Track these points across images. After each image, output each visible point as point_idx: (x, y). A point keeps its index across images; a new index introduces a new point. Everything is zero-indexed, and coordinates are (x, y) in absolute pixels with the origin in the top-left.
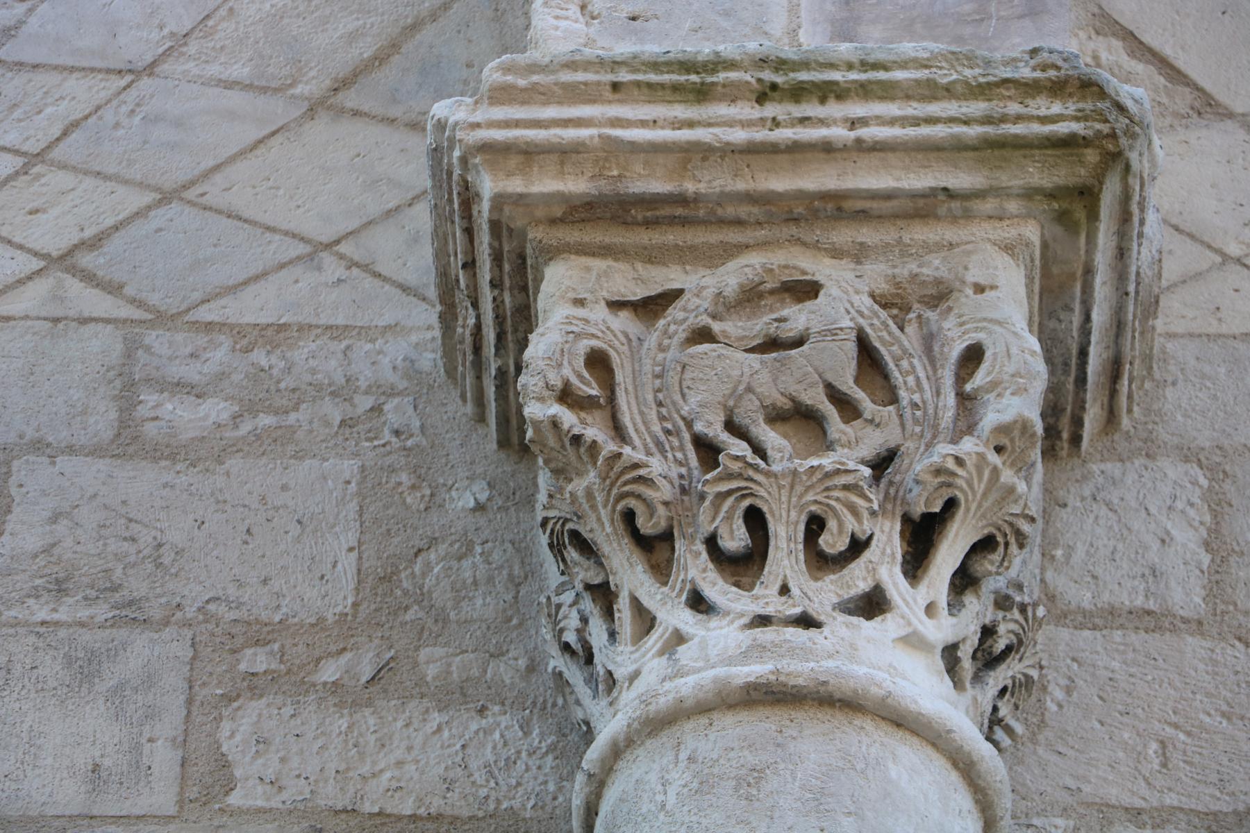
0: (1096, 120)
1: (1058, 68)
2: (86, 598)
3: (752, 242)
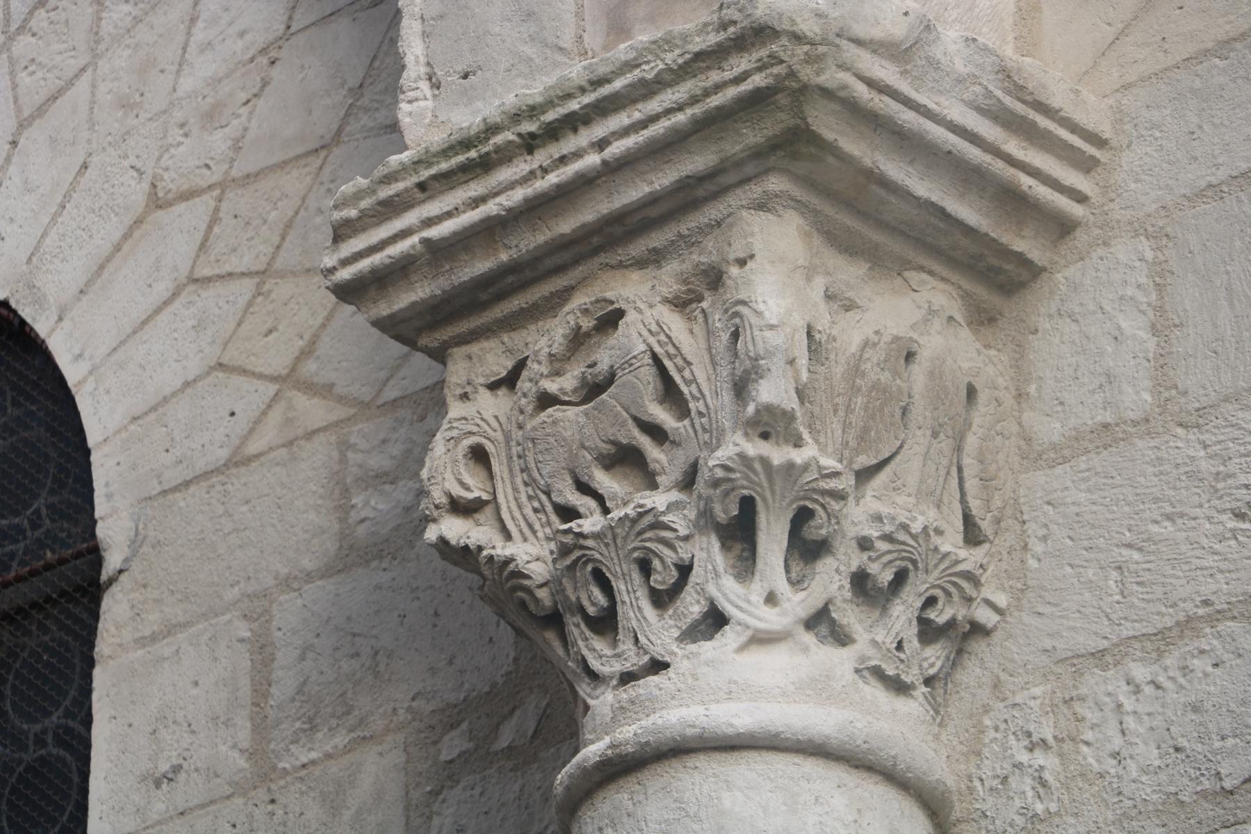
0: (772, 65)
1: (735, 23)
2: (330, 729)
3: (573, 283)
